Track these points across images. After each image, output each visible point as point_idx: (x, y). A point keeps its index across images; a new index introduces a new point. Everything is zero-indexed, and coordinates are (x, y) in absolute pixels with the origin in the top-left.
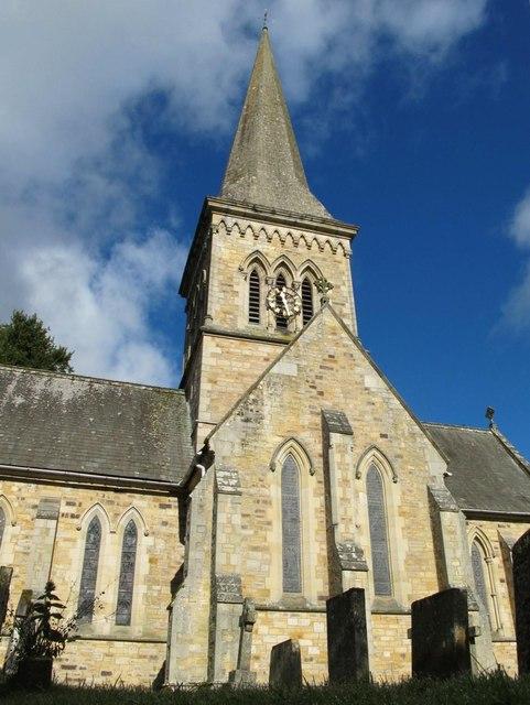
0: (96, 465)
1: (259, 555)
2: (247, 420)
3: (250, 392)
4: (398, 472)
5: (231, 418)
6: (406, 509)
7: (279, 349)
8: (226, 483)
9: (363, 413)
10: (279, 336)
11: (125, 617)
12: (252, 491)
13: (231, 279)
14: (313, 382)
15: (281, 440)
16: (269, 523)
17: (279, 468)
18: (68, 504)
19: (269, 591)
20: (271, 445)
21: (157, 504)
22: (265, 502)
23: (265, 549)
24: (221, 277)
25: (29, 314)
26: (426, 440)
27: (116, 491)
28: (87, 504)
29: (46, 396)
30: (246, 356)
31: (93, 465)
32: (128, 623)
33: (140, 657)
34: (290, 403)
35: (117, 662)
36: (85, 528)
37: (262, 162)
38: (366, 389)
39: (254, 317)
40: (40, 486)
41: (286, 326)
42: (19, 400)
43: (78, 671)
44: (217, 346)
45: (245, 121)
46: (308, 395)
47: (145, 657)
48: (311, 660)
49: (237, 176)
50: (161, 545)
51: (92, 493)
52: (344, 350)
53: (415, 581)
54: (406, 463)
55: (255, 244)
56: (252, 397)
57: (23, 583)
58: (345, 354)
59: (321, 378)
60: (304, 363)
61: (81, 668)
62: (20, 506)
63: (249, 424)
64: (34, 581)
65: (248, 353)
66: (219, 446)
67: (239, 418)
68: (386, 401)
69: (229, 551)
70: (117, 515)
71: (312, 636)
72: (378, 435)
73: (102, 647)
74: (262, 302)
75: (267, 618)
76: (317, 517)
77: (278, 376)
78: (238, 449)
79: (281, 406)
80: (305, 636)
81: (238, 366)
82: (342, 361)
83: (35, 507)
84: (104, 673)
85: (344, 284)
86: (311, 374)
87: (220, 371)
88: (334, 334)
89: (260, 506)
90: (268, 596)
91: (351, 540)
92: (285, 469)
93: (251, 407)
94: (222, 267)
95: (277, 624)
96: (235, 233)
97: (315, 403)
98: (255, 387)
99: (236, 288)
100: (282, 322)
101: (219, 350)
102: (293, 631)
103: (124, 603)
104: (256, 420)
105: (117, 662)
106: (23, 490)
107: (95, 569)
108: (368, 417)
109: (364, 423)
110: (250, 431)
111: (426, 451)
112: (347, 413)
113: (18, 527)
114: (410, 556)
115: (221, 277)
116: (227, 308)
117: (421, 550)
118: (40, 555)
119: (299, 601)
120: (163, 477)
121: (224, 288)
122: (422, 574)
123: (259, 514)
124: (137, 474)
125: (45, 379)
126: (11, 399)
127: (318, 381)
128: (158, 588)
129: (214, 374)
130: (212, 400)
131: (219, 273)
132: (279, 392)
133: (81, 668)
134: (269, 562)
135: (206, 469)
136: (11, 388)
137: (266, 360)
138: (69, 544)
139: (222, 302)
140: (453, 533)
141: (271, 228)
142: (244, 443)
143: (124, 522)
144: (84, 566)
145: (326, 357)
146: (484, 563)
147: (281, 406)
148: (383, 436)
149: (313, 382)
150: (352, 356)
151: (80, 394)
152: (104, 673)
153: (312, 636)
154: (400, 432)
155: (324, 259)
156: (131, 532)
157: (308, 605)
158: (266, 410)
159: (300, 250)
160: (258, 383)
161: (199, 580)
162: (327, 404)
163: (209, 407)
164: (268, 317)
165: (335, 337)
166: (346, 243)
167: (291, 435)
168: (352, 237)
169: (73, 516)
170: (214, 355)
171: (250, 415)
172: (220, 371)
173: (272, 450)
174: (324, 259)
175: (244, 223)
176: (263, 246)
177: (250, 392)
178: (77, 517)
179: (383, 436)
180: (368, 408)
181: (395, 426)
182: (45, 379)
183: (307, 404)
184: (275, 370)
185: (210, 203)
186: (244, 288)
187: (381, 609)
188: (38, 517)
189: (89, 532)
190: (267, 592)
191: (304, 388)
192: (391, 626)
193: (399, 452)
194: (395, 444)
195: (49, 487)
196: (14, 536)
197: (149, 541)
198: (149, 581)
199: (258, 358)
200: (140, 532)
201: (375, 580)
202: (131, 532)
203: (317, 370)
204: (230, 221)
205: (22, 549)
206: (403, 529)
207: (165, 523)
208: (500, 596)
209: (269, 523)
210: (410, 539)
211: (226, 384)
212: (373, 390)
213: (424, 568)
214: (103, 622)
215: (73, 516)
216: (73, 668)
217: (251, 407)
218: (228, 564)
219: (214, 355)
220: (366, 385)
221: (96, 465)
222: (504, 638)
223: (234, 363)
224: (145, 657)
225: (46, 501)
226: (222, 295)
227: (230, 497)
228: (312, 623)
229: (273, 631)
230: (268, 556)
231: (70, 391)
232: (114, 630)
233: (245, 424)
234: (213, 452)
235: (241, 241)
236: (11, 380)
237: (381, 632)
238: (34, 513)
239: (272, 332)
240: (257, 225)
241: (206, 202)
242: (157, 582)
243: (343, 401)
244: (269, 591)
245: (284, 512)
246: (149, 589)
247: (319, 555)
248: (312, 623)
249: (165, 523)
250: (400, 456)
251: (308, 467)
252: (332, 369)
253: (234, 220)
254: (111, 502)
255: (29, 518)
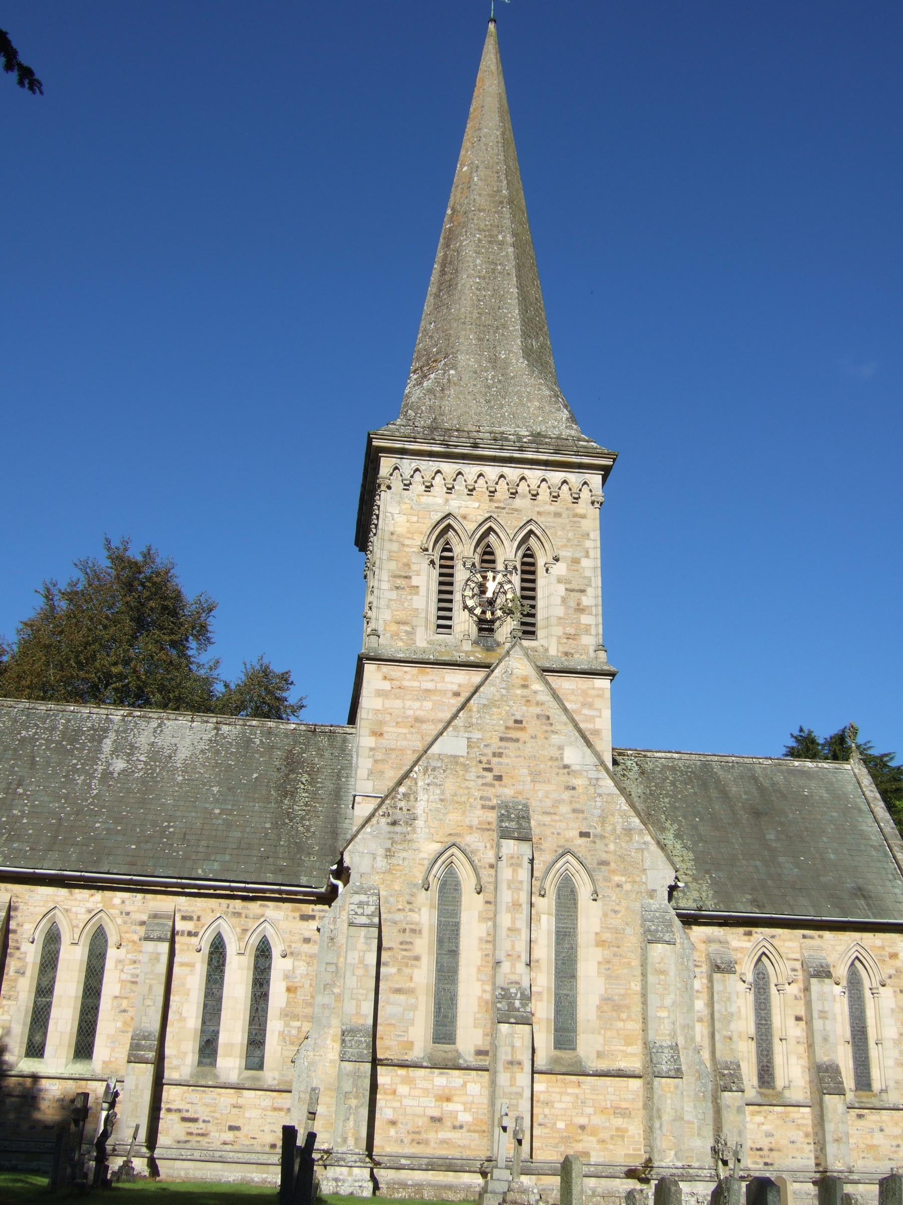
0: (216, 866)
1: (402, 998)
2: (394, 823)
3: (399, 783)
4: (601, 884)
5: (374, 820)
6: (607, 936)
7: (476, 676)
8: (360, 911)
9: (557, 803)
10: (479, 655)
11: (257, 1060)
12: (399, 916)
13: (408, 565)
14: (489, 762)
15: (437, 847)
16: (417, 958)
17: (435, 885)
18: (184, 918)
19: (412, 1043)
20: (422, 855)
21: (297, 915)
22: (413, 931)
23: (411, 992)
24: (393, 565)
25: (135, 554)
26: (648, 838)
27: (244, 899)
28: (207, 919)
29: (155, 753)
30: (427, 691)
31: (212, 867)
32: (260, 1067)
33: (275, 1109)
34: (455, 795)
35: (247, 1115)
36: (206, 949)
37: (467, 338)
38: (566, 767)
39: (444, 622)
40: (149, 896)
41: (491, 630)
42: (119, 765)
43: (200, 1125)
44: (385, 678)
45: (448, 246)
46: (480, 781)
47: (281, 1109)
48: (461, 1127)
49: (430, 362)
50: (302, 968)
51: (213, 902)
52: (538, 710)
53: (609, 1034)
54: (614, 872)
55: (447, 500)
56: (402, 789)
57: (132, 1019)
58: (538, 717)
59: (500, 755)
60: (476, 735)
61: (204, 1121)
62: (125, 923)
63: (398, 829)
64: (144, 1019)
65: (430, 686)
66: (356, 859)
67: (383, 820)
68: (594, 783)
69: (360, 997)
70: (245, 931)
71: (463, 1099)
72: (576, 833)
73: (227, 1097)
74: (457, 597)
75: (408, 1076)
76: (481, 949)
77: (440, 757)
78: (381, 863)
79: (442, 800)
80: (455, 1098)
81: (414, 708)
82: (533, 727)
83: (143, 923)
84: (231, 1128)
85: (587, 556)
86: (486, 751)
87: (388, 718)
88: (525, 686)
89: (407, 937)
90: (411, 1049)
91: (517, 983)
92: (444, 885)
93: (402, 804)
94: (395, 547)
95: (421, 1084)
96: (418, 487)
97: (490, 792)
98: (406, 776)
99: (415, 581)
100: (486, 627)
101: (386, 685)
102: (441, 1092)
103: (256, 1042)
104: (407, 823)
105: (247, 1115)
106: (127, 902)
107: (220, 1000)
108: (564, 809)
109: (557, 818)
110: (398, 838)
111: (646, 854)
112: (534, 804)
113: (123, 950)
114: (606, 999)
115: (393, 565)
116: (401, 615)
117: (623, 992)
118: (150, 987)
119: (450, 1055)
120: (304, 880)
121: (399, 582)
122: (620, 1024)
123: (404, 947)
124: (270, 877)
125: (154, 724)
126: (109, 764)
127: (495, 760)
128: (298, 1024)
129: (381, 722)
130: (376, 761)
131: (390, 559)
132: (438, 781)
133: (204, 1121)
134: (414, 1008)
135: (345, 885)
136: (107, 745)
137: (457, 694)
138: (187, 970)
139: (394, 605)
140: (662, 972)
141: (471, 470)
142: (389, 854)
143: (255, 940)
144: (206, 997)
145: (511, 723)
146: (14, 1177)
147: (442, 800)
148: (584, 835)
149: (489, 762)
150: (548, 718)
151: (202, 746)
152: (231, 1128)
153: (463, 1099)
154: (609, 828)
155: (558, 515)
156: (263, 952)
157: (461, 1061)
158: (420, 808)
159: (518, 502)
160: (411, 770)
161: (326, 1030)
162: (507, 792)
163: (371, 773)
164: (463, 622)
165: (525, 692)
166: (596, 479)
167: (453, 839)
168: (606, 471)
169: (190, 934)
170: (380, 693)
171: (399, 815)
172: (388, 718)
173: (426, 863)
174: (558, 515)
175: (428, 466)
176: (459, 504)
177: (399, 783)
178: (196, 934)
179: (584, 835)
180: (566, 795)
181: (603, 820)
182: (154, 724)
183: (478, 794)
184: (435, 749)
185: (376, 443)
186: (426, 579)
187: (558, 1069)
188: (147, 939)
189: (211, 953)
190: (410, 1045)
191: (475, 770)
192: (570, 1090)
193: (604, 856)
194: (600, 845)
195: (159, 897)
196: (119, 961)
197: (288, 963)
198: (287, 1015)
199: (445, 692)
200: (276, 952)
201: (556, 1030)
202: (263, 952)
203: (495, 744)
204: (407, 465)
205: (129, 978)
206: (599, 963)
207: (307, 940)
208: (792, 1041)
209: (417, 958)
210: (608, 977)
211: (395, 735)
212: (577, 768)
213: (624, 1016)
214: (230, 1063)
215: (190, 934)
216: (194, 1120)
217: (402, 804)
218: (358, 1013)
219: (380, 693)
220: (566, 761)
221: (216, 866)
222: (788, 1102)
223: (408, 704)
224: (281, 1109)
225: (155, 916)
226: (394, 595)
227: (363, 931)
228: (464, 1085)
229: (416, 1092)
230: (413, 1001)
231: (188, 742)
232: (243, 1076)
233: (391, 828)
234: (348, 868)
235: (426, 499)
236: (106, 730)
237: (556, 1097)
238: (142, 931)
239: (468, 651)
240: (449, 468)
241: (370, 441)
242: (296, 1017)
243: (529, 786)
244: (412, 1043)
245: (440, 941)
246: (287, 1025)
247: (480, 998)
248: (464, 1085)
249: (307, 940)
250: (605, 863)
251: (473, 881)
252: (517, 740)
253: (414, 465)
254: (238, 914)
255: (136, 937)
